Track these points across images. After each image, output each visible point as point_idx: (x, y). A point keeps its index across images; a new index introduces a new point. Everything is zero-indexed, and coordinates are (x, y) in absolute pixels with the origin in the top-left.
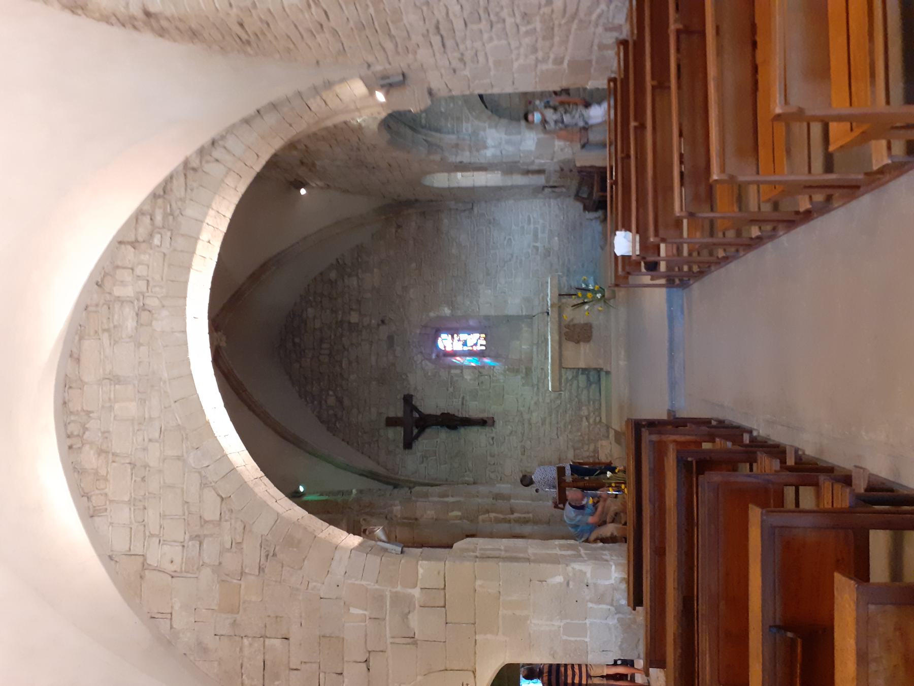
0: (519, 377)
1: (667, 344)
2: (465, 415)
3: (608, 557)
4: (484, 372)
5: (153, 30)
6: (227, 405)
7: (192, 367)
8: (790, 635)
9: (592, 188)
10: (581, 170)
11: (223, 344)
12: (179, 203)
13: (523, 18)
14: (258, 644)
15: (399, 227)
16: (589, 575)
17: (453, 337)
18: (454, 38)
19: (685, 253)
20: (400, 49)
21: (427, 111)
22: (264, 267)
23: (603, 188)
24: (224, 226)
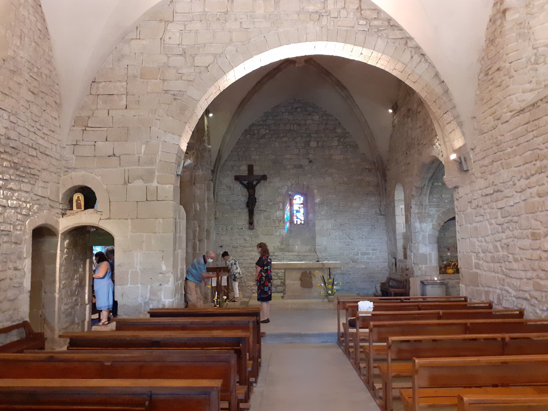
0: (279, 244)
1: (303, 333)
2: (255, 212)
3: (177, 297)
4: (281, 223)
5: (494, 15)
6: (262, 68)
7: (285, 46)
8: (147, 403)
9: (398, 288)
10: (407, 282)
11: (297, 65)
12: (385, 35)
13: (505, 244)
14: (123, 91)
15: (369, 170)
16: (166, 286)
17: (302, 204)
18: (492, 201)
19: (361, 344)
20: (484, 168)
21: (444, 184)
22: (343, 88)
23: (396, 295)
24: (371, 62)
